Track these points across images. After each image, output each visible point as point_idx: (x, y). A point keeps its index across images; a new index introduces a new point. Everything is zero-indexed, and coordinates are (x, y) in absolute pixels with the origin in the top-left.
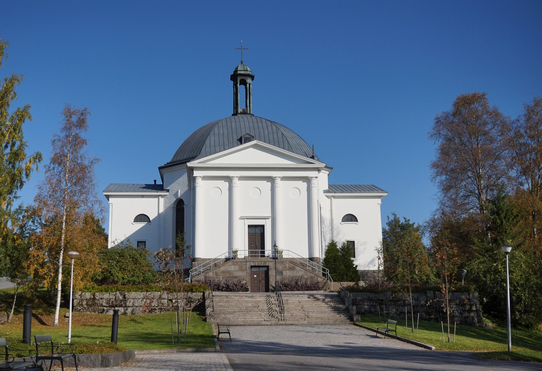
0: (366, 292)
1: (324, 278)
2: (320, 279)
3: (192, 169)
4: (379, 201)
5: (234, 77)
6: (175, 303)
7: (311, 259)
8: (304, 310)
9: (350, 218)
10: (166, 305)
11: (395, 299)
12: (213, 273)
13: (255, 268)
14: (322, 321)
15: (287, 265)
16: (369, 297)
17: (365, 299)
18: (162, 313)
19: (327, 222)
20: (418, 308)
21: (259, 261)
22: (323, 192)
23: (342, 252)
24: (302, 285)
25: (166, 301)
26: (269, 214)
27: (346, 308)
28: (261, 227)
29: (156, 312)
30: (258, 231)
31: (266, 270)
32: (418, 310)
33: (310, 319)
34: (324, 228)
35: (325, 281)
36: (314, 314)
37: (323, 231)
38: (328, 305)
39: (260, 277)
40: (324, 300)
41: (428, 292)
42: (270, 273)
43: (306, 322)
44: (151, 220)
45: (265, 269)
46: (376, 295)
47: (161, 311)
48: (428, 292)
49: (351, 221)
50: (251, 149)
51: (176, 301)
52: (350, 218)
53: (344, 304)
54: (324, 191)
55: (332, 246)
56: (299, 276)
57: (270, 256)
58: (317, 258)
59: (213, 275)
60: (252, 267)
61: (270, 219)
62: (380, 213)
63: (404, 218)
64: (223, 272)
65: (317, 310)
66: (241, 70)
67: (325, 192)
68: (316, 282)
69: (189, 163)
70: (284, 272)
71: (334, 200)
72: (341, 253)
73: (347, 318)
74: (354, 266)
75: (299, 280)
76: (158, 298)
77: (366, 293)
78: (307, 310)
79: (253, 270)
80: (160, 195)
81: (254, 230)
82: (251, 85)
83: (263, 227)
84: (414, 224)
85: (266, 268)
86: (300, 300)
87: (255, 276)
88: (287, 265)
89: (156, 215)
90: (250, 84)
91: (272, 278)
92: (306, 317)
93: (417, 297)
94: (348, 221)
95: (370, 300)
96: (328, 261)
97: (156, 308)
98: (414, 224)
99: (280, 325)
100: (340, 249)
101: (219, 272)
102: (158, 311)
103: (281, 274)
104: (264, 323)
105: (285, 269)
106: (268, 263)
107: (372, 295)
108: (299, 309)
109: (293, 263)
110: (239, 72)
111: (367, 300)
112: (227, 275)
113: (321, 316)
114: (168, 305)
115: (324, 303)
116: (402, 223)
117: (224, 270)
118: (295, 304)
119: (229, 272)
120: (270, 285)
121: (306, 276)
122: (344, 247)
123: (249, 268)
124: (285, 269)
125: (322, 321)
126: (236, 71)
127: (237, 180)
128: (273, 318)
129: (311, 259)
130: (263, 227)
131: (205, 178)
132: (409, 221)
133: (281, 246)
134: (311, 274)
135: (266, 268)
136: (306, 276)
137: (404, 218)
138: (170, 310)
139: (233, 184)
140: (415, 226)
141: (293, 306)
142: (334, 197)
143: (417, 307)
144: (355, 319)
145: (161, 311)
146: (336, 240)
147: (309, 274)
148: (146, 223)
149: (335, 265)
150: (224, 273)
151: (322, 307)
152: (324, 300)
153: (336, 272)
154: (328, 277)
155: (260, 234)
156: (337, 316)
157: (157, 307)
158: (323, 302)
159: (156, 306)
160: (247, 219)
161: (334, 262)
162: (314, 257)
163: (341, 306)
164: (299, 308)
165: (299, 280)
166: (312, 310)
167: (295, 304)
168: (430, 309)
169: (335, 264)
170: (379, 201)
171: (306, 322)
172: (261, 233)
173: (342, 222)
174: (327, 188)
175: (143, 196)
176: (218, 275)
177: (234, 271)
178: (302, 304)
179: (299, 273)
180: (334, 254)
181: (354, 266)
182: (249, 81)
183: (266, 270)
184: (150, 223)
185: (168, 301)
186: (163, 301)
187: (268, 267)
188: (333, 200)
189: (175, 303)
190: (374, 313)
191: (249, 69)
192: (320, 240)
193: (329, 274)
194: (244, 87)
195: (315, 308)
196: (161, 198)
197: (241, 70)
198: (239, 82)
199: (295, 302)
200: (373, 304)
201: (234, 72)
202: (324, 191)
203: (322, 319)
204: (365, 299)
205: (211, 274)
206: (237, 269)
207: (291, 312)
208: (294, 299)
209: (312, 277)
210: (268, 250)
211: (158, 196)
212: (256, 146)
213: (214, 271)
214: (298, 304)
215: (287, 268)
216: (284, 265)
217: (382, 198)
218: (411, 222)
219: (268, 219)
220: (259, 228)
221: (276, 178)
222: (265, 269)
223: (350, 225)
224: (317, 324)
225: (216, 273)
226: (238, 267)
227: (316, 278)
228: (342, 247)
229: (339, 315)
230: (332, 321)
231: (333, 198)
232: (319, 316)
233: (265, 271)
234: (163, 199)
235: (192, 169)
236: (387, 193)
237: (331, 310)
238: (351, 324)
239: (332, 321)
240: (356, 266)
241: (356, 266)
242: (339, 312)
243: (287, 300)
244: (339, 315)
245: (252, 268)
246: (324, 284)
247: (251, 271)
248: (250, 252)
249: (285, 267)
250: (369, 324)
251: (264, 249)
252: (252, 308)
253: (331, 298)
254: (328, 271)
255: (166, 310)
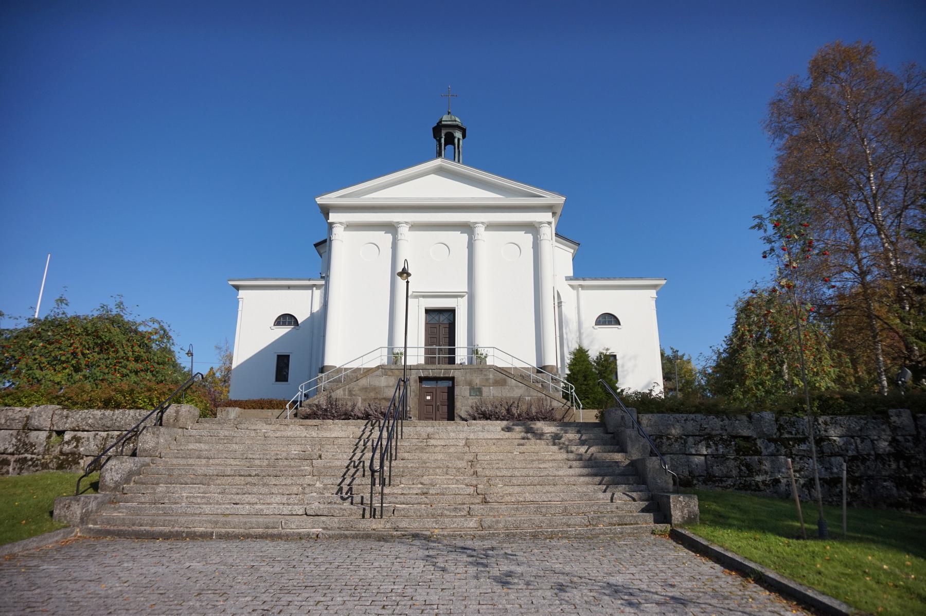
0: (691, 413)
1: (565, 401)
2: (555, 404)
3: (326, 210)
4: (653, 293)
5: (437, 130)
6: (68, 443)
7: (542, 369)
8: (475, 473)
9: (608, 319)
10: (40, 449)
11: (787, 436)
12: (344, 390)
13: (429, 382)
14: (537, 518)
15: (491, 376)
16: (702, 429)
17: (688, 436)
18: (25, 474)
19: (573, 326)
20: (868, 463)
21: (440, 370)
22: (565, 279)
23: (598, 367)
24: (520, 415)
25: (43, 435)
26: (464, 288)
27: (633, 464)
28: (450, 313)
29: (8, 472)
30: (443, 318)
31: (451, 385)
32: (870, 473)
33: (492, 509)
34: (569, 334)
35: (566, 406)
36: (510, 490)
37: (567, 339)
38: (571, 456)
39: (438, 400)
40: (556, 438)
41: (892, 412)
42: (457, 391)
43: (472, 523)
44: (299, 323)
45: (448, 384)
46: (726, 422)
47: (21, 469)
48: (892, 412)
49: (610, 323)
50: (433, 176)
51: (74, 438)
52: (608, 319)
53: (623, 450)
54: (566, 277)
55: (580, 355)
56: (514, 398)
57: (464, 363)
58: (552, 367)
59: (344, 394)
60: (421, 379)
61: (466, 298)
62: (655, 311)
63: (672, 348)
64: (365, 389)
65: (524, 472)
66: (446, 121)
67: (568, 279)
68: (548, 410)
69: (318, 198)
70: (485, 390)
71: (582, 293)
72: (596, 368)
73: (643, 504)
74: (619, 391)
75: (516, 405)
76: (20, 426)
77: (692, 416)
78: (487, 472)
79: (424, 386)
80: (314, 285)
81: (437, 318)
82: (461, 141)
83: (452, 312)
84: (684, 355)
85: (451, 382)
86: (472, 436)
87: (429, 398)
88: (491, 376)
89: (308, 315)
90: (459, 140)
91: (460, 401)
92: (478, 499)
93: (860, 430)
94: (604, 323)
95: (708, 438)
96: (574, 378)
97: (9, 457)
98: (684, 355)
99: (367, 537)
100: (595, 362)
101: (356, 388)
102: (14, 469)
103: (478, 393)
104: (294, 526)
105: (488, 384)
106: (454, 372)
107: (714, 424)
108: (458, 469)
109: (504, 375)
110: (443, 123)
111: (698, 438)
112: (372, 395)
113: (537, 498)
114: (47, 451)
115: (556, 448)
116: (668, 356)
117: (366, 384)
118: (452, 450)
119: (375, 389)
120: (456, 415)
121: (529, 398)
122: (601, 359)
123: (416, 381)
124: (488, 384)
125: (537, 518)
126: (441, 122)
127: (408, 229)
128: (347, 504)
129: (542, 369)
130: (452, 312)
131: (350, 227)
132: (678, 351)
133: (483, 341)
134: (540, 395)
135: (451, 382)
136: (529, 398)
137: (672, 348)
138: (51, 465)
139: (399, 235)
140: (685, 358)
141: (440, 457)
142: (582, 287)
143: (864, 461)
144: (677, 515)
145: (21, 469)
146: (585, 346)
147: (534, 393)
148: (292, 327)
149: (586, 385)
150: (366, 391)
151: (544, 462)
152: (556, 438)
153: (588, 398)
154: (572, 398)
155: (447, 326)
156: (601, 495)
157: (12, 454)
158: (554, 444)
159: (10, 450)
160: (424, 297)
161: (584, 381)
162: (546, 364)
163: (618, 457)
164: (461, 464)
165: (516, 405)
166: (504, 472)
167: (452, 450)
168: (908, 468)
169: (586, 383)
170: (653, 293)
171: (472, 523)
172: (449, 324)
173: (596, 325)
174: (571, 274)
175: (289, 287)
176: (354, 395)
177: (387, 387)
178: (474, 449)
179: (514, 391)
180: (584, 367)
181: (619, 391)
182: (458, 134)
183: (451, 385)
184: (297, 327)
185: (49, 437)
186: (33, 434)
187: (452, 379)
188: (582, 292)
189: (68, 443)
190: (721, 481)
191: (457, 119)
192: (558, 334)
193: (574, 394)
194: (453, 147)
195: (517, 465)
196: (316, 289)
197: (446, 121)
198: (444, 137)
199: (452, 442)
200: (717, 450)
201: (438, 124)
202: (566, 277)
203: (537, 511)
204: (688, 436)
205: (339, 393)
206: (391, 384)
207: (426, 479)
208: (452, 434)
209: (539, 399)
210: (461, 355)
211: (310, 287)
212: (440, 171)
213: (347, 387)
214: (460, 449)
215: (491, 381)
216: (485, 375)
217: (658, 289)
218: (680, 354)
219: (462, 296)
220: (446, 315)
221: (477, 225)
222: (448, 384)
223: (608, 331)
224: (514, 535)
225: (350, 391)
226: (394, 380)
227: (549, 402)
228: (597, 359)
229: (609, 494)
230: (578, 519)
231: (580, 289)
232: (529, 497)
233: (449, 388)
234: (319, 291)
235: (326, 210)
236: (665, 281)
237: (585, 471)
238: (662, 534)
239: (578, 519)
240: (622, 391)
241: (622, 391)
242: (606, 479)
243: (429, 437)
244: (608, 495)
245: (424, 382)
246: (564, 412)
247: (421, 388)
248: (426, 359)
249: (487, 380)
250: (780, 545)
251: (454, 354)
252: (292, 463)
253: (578, 432)
254: (572, 388)
255: (37, 466)
